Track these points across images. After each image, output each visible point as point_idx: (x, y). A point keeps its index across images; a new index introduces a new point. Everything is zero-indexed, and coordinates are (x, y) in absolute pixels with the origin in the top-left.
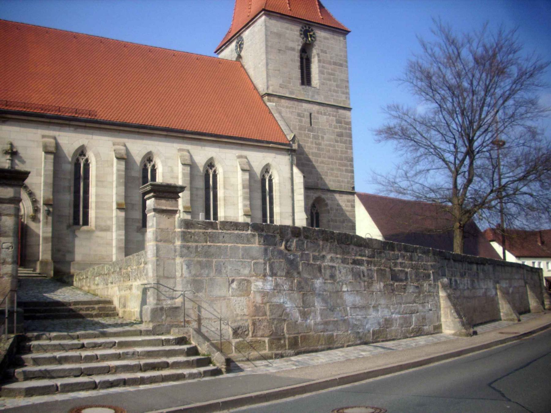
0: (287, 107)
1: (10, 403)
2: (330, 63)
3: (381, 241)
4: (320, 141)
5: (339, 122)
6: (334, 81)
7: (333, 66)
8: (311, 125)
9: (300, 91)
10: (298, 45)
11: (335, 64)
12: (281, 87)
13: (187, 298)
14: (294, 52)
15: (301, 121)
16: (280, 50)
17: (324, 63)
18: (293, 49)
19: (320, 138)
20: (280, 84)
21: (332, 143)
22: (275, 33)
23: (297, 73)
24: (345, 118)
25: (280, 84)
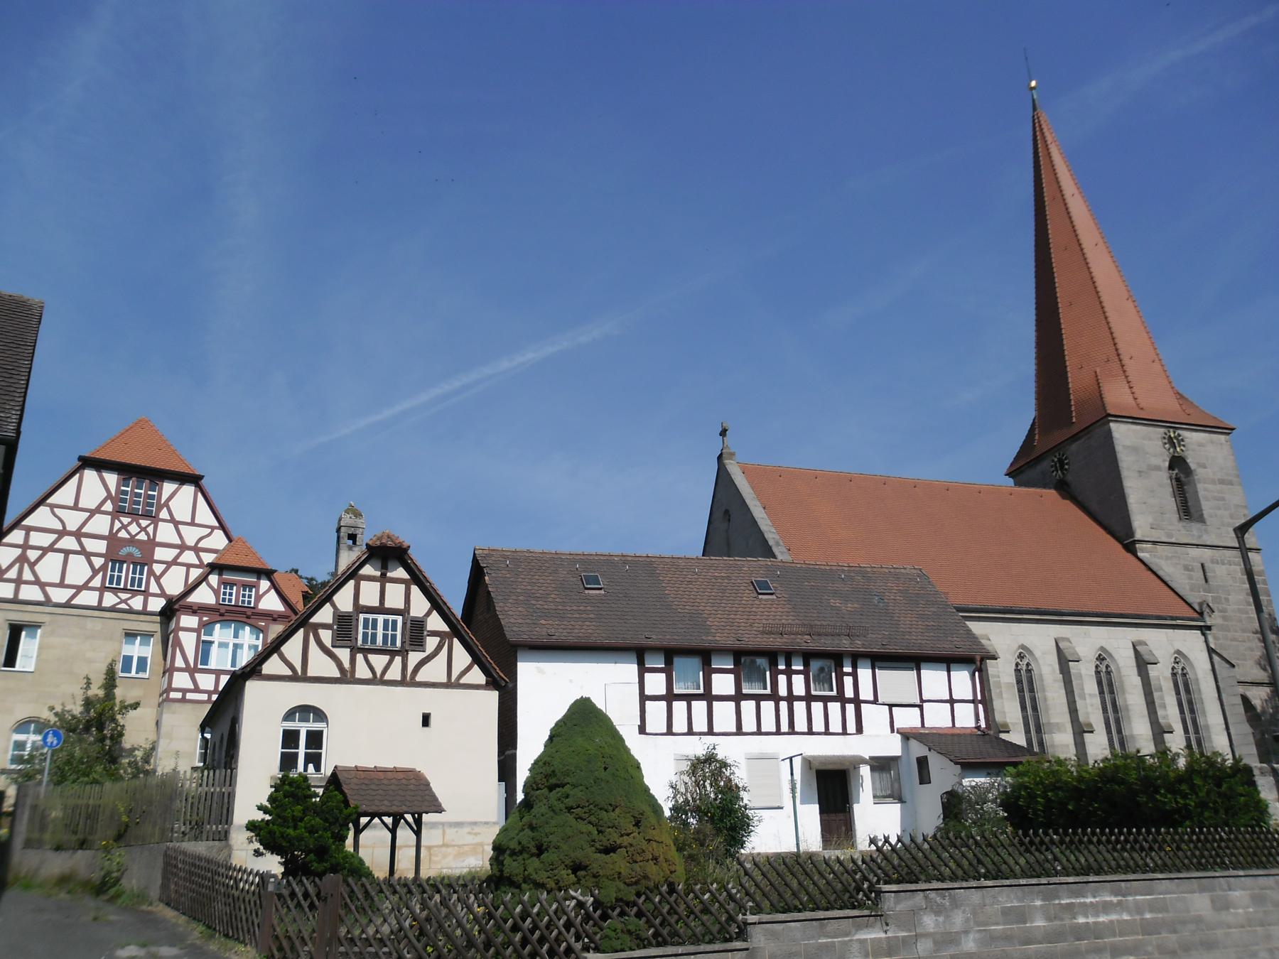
0: (1167, 558)
2: (1213, 482)
4: (1224, 606)
6: (1226, 509)
7: (1219, 487)
10: (1164, 461)
11: (1222, 482)
12: (1151, 528)
14: (1159, 473)
15: (1190, 578)
17: (1205, 483)
18: (1158, 468)
19: (1223, 600)
20: (1151, 524)
21: (1242, 607)
22: (1129, 447)
23: (1170, 504)
25: (1151, 524)
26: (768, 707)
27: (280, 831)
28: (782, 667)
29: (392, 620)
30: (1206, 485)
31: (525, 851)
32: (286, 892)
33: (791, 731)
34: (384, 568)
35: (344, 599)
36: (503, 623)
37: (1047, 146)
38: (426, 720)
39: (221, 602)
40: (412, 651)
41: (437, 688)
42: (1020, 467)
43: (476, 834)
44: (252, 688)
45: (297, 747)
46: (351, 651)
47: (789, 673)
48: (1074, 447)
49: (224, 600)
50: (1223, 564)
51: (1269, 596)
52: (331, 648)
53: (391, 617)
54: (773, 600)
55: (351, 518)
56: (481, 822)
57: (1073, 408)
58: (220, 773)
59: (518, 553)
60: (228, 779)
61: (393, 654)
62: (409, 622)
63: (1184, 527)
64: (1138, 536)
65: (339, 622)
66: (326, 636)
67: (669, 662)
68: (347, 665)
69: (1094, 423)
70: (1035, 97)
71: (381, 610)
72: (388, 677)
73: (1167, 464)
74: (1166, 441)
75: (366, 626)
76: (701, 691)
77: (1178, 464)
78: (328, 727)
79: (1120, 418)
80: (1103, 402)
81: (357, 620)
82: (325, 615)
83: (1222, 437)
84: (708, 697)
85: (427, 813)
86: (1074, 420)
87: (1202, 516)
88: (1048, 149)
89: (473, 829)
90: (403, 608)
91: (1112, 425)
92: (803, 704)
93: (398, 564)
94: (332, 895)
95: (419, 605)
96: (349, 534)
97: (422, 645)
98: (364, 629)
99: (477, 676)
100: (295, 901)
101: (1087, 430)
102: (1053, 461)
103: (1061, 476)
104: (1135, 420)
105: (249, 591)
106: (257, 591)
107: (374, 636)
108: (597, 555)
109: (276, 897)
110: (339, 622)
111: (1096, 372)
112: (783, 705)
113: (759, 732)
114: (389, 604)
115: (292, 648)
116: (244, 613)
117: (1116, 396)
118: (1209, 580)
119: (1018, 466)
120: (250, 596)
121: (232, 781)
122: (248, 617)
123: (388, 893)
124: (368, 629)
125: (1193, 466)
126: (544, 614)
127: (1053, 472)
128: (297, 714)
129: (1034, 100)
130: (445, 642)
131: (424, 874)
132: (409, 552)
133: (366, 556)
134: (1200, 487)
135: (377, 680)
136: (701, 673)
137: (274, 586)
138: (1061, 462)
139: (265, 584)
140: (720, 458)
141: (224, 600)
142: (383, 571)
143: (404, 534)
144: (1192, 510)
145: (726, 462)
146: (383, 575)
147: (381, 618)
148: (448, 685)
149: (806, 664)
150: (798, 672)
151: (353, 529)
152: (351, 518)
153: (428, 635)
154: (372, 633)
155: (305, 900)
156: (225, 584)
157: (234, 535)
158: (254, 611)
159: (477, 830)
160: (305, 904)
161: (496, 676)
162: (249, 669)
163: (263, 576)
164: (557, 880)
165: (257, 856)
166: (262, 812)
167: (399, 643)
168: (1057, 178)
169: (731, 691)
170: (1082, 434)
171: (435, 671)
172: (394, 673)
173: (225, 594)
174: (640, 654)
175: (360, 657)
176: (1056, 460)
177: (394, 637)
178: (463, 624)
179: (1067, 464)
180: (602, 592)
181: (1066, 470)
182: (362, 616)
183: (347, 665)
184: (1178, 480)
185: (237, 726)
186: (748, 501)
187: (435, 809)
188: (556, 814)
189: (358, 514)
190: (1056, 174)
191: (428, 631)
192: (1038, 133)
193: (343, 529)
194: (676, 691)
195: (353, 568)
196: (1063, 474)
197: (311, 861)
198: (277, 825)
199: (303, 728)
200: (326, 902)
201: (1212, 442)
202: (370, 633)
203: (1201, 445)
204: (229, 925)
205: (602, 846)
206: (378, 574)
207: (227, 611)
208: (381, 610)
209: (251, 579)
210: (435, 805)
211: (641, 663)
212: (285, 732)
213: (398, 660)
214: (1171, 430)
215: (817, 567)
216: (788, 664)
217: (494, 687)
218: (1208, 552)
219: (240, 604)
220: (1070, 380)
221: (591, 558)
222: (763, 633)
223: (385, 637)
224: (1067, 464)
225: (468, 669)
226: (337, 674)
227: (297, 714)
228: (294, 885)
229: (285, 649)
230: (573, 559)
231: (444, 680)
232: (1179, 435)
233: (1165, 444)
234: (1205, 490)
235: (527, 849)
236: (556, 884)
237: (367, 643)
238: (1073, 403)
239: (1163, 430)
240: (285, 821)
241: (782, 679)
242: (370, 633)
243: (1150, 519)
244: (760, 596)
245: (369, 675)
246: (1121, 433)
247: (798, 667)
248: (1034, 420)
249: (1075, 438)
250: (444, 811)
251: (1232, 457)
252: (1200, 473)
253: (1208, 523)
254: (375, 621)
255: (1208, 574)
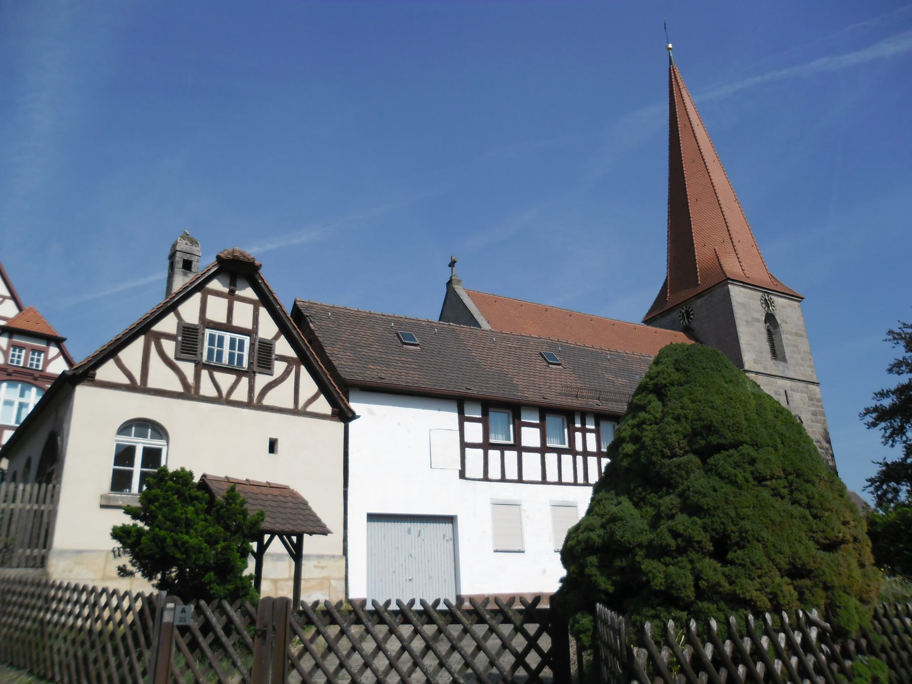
1: (11, 573)
3: (242, 571)
5: (811, 399)
7: (794, 337)
8: (788, 403)
9: (771, 366)
10: (762, 316)
11: (796, 334)
12: (755, 363)
13: (335, 579)
16: (747, 322)
18: (758, 320)
21: (809, 423)
23: (766, 347)
24: (815, 395)
25: (754, 360)
26: (567, 459)
27: (172, 537)
28: (578, 425)
29: (239, 340)
30: (787, 336)
31: (693, 547)
32: (195, 625)
33: (585, 482)
34: (233, 284)
35: (190, 311)
36: (335, 364)
37: (680, 89)
38: (273, 446)
39: (9, 363)
40: (260, 373)
41: (284, 414)
42: (654, 317)
43: (323, 568)
44: (82, 394)
45: (132, 464)
46: (195, 366)
47: (584, 431)
48: (699, 302)
49: (12, 361)
50: (798, 392)
51: (824, 416)
52: (175, 361)
53: (238, 337)
54: (560, 369)
55: (186, 244)
56: (328, 556)
57: (699, 274)
58: (32, 488)
59: (336, 309)
60: (49, 495)
61: (240, 373)
62: (257, 344)
63: (774, 363)
64: (747, 367)
65: (184, 334)
66: (169, 347)
67: (485, 413)
68: (191, 380)
69: (717, 284)
70: (671, 55)
71: (228, 327)
72: (234, 397)
73: (764, 318)
74: (763, 302)
75: (211, 342)
76: (512, 442)
77: (770, 319)
78: (168, 445)
79: (736, 281)
80: (722, 270)
81: (203, 334)
82: (168, 324)
83: (796, 303)
84: (517, 447)
85: (311, 534)
86: (699, 283)
87: (785, 357)
88: (680, 92)
89: (319, 563)
90: (251, 328)
91: (729, 286)
92: (595, 458)
93: (246, 283)
94: (274, 628)
95: (268, 328)
96: (184, 260)
97: (270, 369)
98: (209, 345)
99: (323, 405)
100: (211, 637)
101: (709, 289)
102: (681, 312)
103: (687, 323)
104: (745, 284)
105: (38, 356)
106: (46, 357)
107: (220, 354)
108: (406, 318)
109: (176, 632)
110: (184, 334)
111: (715, 250)
112: (580, 459)
113: (560, 483)
114: (236, 322)
115: (132, 355)
116: (31, 375)
117: (731, 266)
118: (790, 402)
119: (655, 314)
120: (38, 360)
121: (54, 498)
122: (36, 379)
123: (467, 622)
124: (214, 346)
125: (779, 321)
126: (371, 361)
127: (681, 320)
128: (134, 428)
129: (670, 57)
130: (292, 369)
131: (351, 597)
132: (261, 271)
133: (216, 269)
134: (783, 336)
135: (222, 399)
136: (511, 426)
137: (63, 353)
138: (688, 313)
139: (53, 351)
140: (449, 283)
141: (12, 361)
142: (232, 287)
143: (252, 251)
144: (778, 353)
145: (455, 286)
146: (232, 292)
147: (227, 336)
148: (295, 412)
149: (597, 424)
150: (591, 431)
151: (188, 255)
152: (186, 244)
153: (276, 359)
154: (217, 350)
155: (228, 633)
156: (15, 346)
157: (25, 304)
158: (41, 373)
159: (323, 563)
160: (204, 643)
161: (343, 407)
162: (81, 371)
163: (52, 343)
164: (771, 593)
165: (122, 576)
166: (129, 516)
167: (245, 364)
168: (687, 112)
169: (537, 444)
170: (706, 292)
171: (281, 396)
172: (241, 394)
173: (13, 356)
174: (460, 402)
175: (205, 373)
176: (684, 311)
177: (240, 357)
178: (312, 351)
179: (692, 314)
180: (418, 348)
181: (691, 319)
182: (208, 332)
183: (191, 380)
184: (768, 331)
185: (59, 438)
186: (476, 316)
187: (321, 529)
188: (740, 488)
189: (193, 242)
190: (686, 110)
191: (276, 355)
192: (673, 80)
193: (178, 254)
194: (492, 441)
195: (202, 279)
196: (689, 321)
197: (210, 583)
198: (166, 529)
199: (140, 444)
200: (265, 638)
201: (790, 306)
202: (216, 350)
203: (784, 307)
204: (83, 673)
205: (826, 538)
206: (226, 290)
207: (15, 372)
208: (228, 327)
209: (41, 345)
210: (319, 526)
211: (461, 412)
212: (118, 446)
213: (245, 381)
214: (766, 295)
215: (586, 348)
216: (583, 423)
217: (339, 417)
218: (788, 383)
219: (28, 366)
220: (696, 254)
221: (401, 320)
222: (561, 394)
223: (231, 356)
224: (692, 314)
225: (315, 398)
226: (179, 388)
227: (134, 428)
228: (209, 613)
229: (123, 355)
230: (386, 320)
231: (291, 406)
232: (771, 299)
233: (763, 304)
234: (787, 339)
235: (696, 545)
236: (771, 600)
237: (213, 360)
238: (698, 270)
239: (761, 294)
240: (177, 525)
241: (578, 436)
242: (216, 350)
243: (754, 356)
244: (550, 366)
245: (213, 393)
246: (736, 293)
247: (590, 426)
248: (666, 280)
249: (700, 295)
250: (330, 532)
251: (802, 318)
252: (784, 327)
253: (788, 362)
254: (221, 339)
255: (789, 398)
